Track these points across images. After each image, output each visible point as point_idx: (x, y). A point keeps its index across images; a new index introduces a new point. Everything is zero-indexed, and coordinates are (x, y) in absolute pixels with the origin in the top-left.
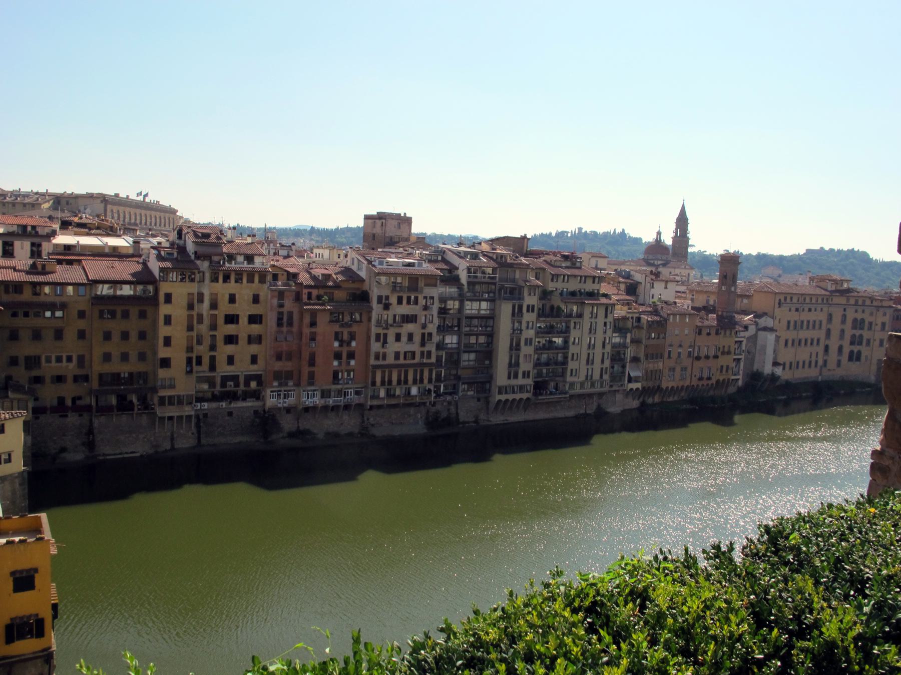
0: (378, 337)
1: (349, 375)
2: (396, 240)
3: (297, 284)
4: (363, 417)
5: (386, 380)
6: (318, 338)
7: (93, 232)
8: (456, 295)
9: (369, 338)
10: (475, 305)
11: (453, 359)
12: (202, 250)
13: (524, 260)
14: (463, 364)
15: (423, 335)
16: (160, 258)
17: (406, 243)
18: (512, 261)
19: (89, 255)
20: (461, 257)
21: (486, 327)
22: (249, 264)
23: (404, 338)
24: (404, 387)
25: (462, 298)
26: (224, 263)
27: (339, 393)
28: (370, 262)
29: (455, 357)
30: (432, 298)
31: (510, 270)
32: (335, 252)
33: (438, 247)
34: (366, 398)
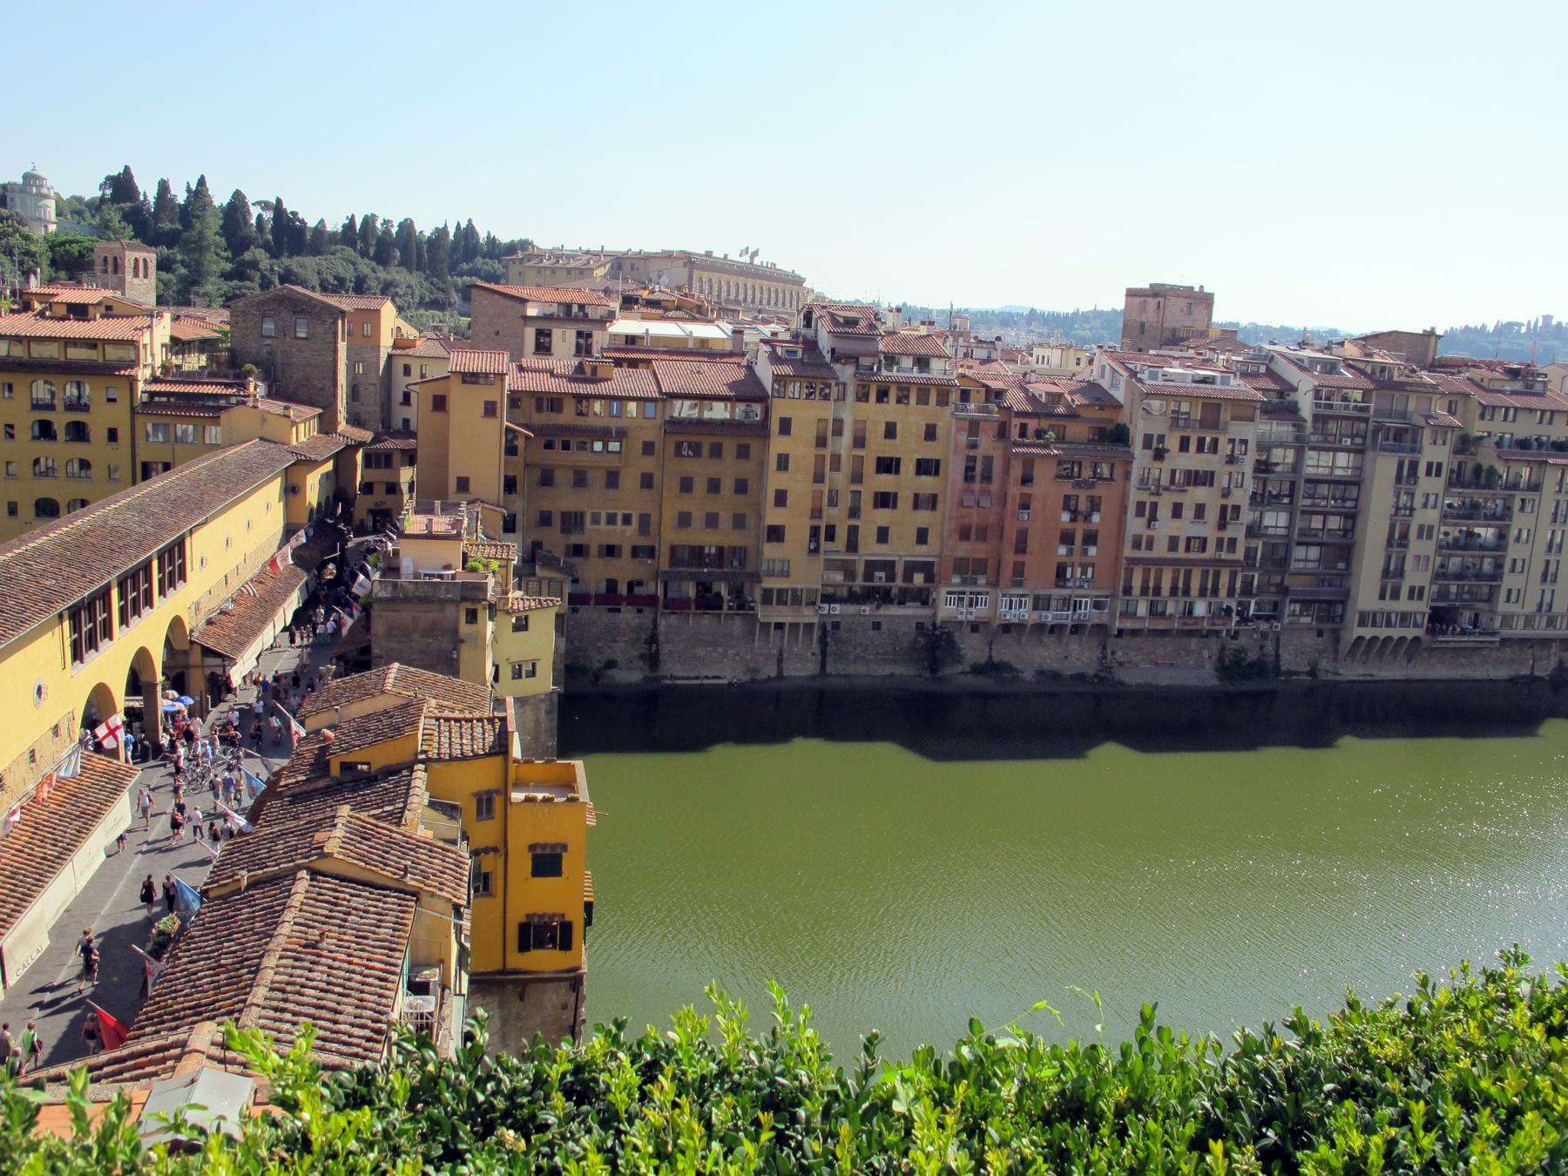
1: (1084, 572)
2: (1182, 334)
5: (1151, 585)
7: (670, 314)
8: (1291, 439)
10: (1326, 458)
11: (1277, 556)
12: (845, 346)
13: (1426, 377)
14: (1295, 566)
15: (1224, 508)
16: (775, 359)
17: (1202, 342)
18: (1403, 379)
19: (664, 352)
21: (1344, 500)
22: (921, 371)
23: (1188, 513)
24: (1182, 600)
26: (879, 369)
27: (1065, 602)
28: (1133, 374)
29: (1281, 553)
30: (1245, 442)
31: (1397, 394)
33: (1261, 349)
34: (1112, 615)
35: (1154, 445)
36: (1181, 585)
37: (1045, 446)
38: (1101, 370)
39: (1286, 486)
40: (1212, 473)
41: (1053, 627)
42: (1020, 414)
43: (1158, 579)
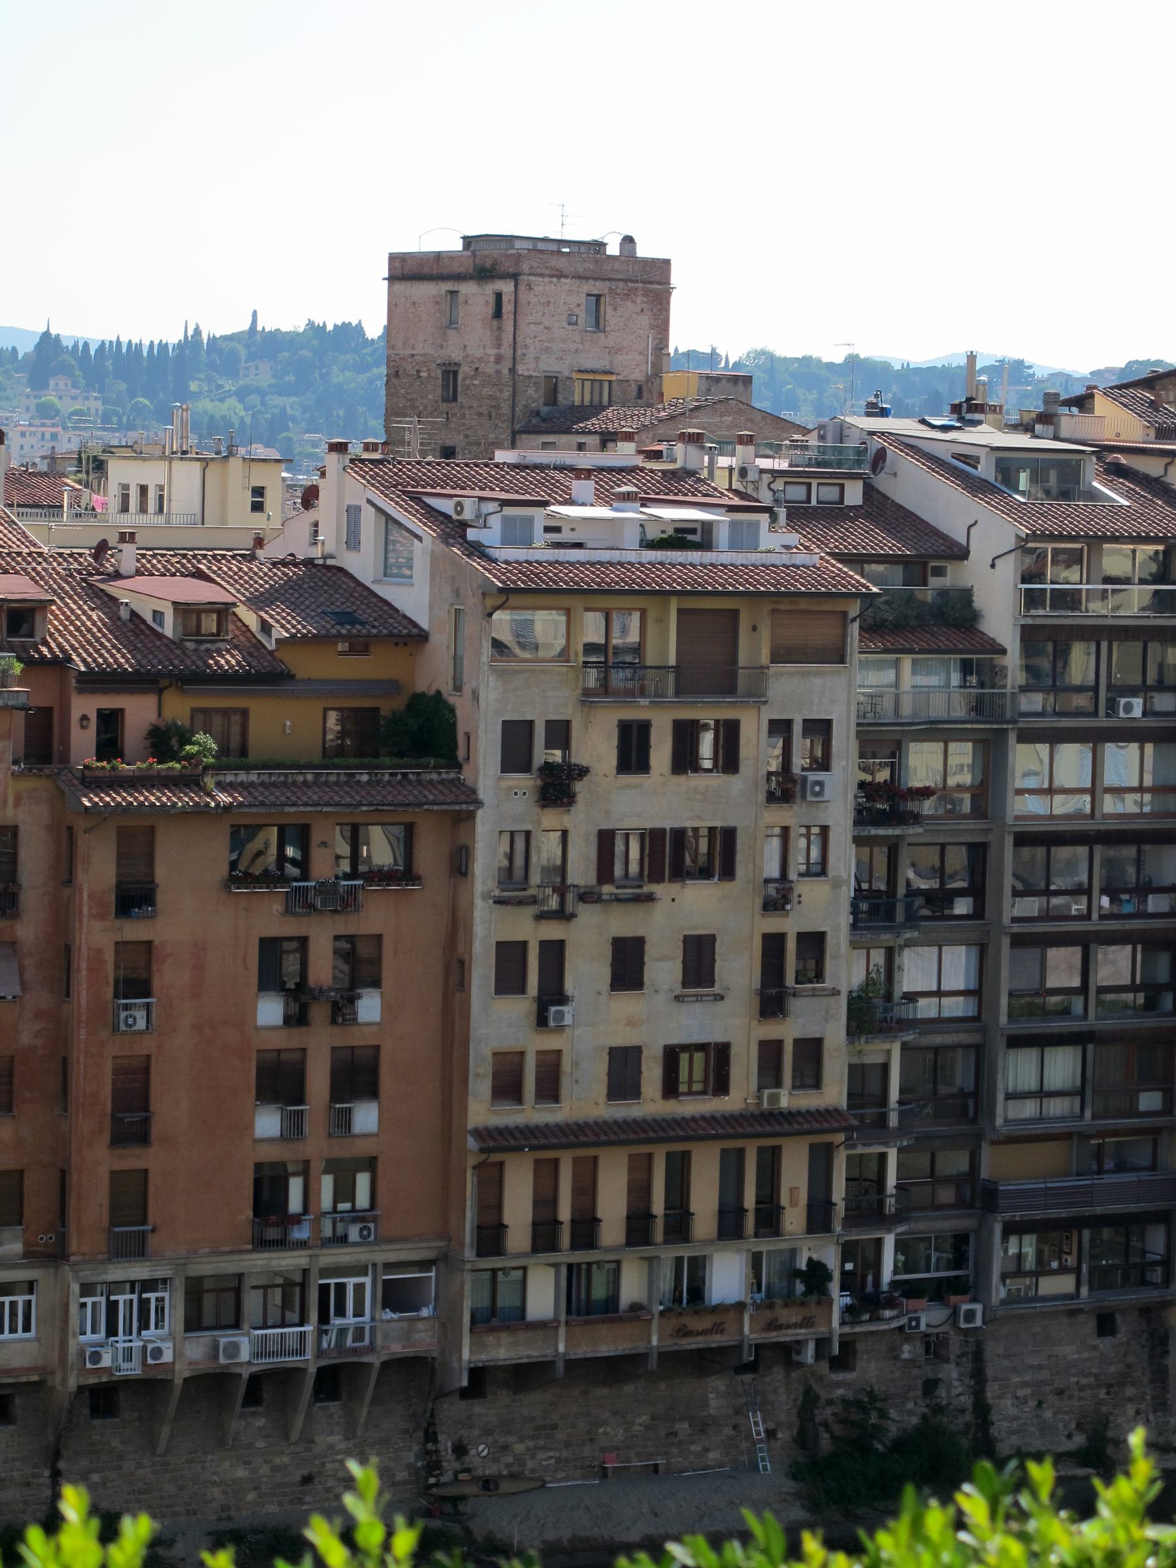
0: (510, 958)
1: (344, 1191)
2: (578, 395)
3: (33, 664)
4: (431, 1436)
5: (565, 1213)
6: (169, 977)
8: (960, 711)
9: (456, 972)
10: (1072, 762)
11: (953, 1088)
14: (1010, 1113)
15: (773, 945)
20: (977, 487)
21: (1144, 889)
23: (663, 969)
24: (668, 1254)
25: (991, 731)
27: (293, 1294)
28: (453, 530)
29: (962, 1075)
30: (820, 729)
32: (235, 482)
33: (842, 432)
34: (447, 1323)
35: (542, 754)
36: (658, 1206)
37: (189, 782)
38: (347, 523)
39: (957, 859)
40: (729, 835)
41: (256, 1380)
42: (99, 680)
43: (586, 1191)
